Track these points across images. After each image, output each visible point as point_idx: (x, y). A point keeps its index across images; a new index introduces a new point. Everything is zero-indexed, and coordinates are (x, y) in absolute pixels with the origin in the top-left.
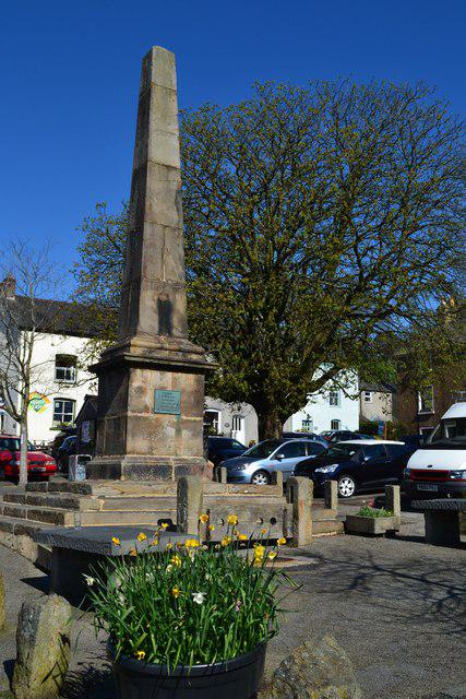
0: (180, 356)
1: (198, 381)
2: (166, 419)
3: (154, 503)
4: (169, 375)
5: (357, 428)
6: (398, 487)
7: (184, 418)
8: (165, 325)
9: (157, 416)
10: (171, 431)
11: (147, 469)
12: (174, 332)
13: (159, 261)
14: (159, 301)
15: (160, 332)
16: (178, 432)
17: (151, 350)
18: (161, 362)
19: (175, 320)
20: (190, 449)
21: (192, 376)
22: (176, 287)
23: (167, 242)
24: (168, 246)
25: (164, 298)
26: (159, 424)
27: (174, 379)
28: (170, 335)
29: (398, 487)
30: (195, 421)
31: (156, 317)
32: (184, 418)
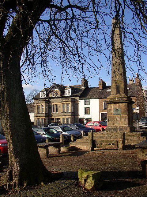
0: (120, 99)
1: (125, 105)
10: (118, 119)
16: (121, 119)
17: (112, 99)
21: (124, 104)
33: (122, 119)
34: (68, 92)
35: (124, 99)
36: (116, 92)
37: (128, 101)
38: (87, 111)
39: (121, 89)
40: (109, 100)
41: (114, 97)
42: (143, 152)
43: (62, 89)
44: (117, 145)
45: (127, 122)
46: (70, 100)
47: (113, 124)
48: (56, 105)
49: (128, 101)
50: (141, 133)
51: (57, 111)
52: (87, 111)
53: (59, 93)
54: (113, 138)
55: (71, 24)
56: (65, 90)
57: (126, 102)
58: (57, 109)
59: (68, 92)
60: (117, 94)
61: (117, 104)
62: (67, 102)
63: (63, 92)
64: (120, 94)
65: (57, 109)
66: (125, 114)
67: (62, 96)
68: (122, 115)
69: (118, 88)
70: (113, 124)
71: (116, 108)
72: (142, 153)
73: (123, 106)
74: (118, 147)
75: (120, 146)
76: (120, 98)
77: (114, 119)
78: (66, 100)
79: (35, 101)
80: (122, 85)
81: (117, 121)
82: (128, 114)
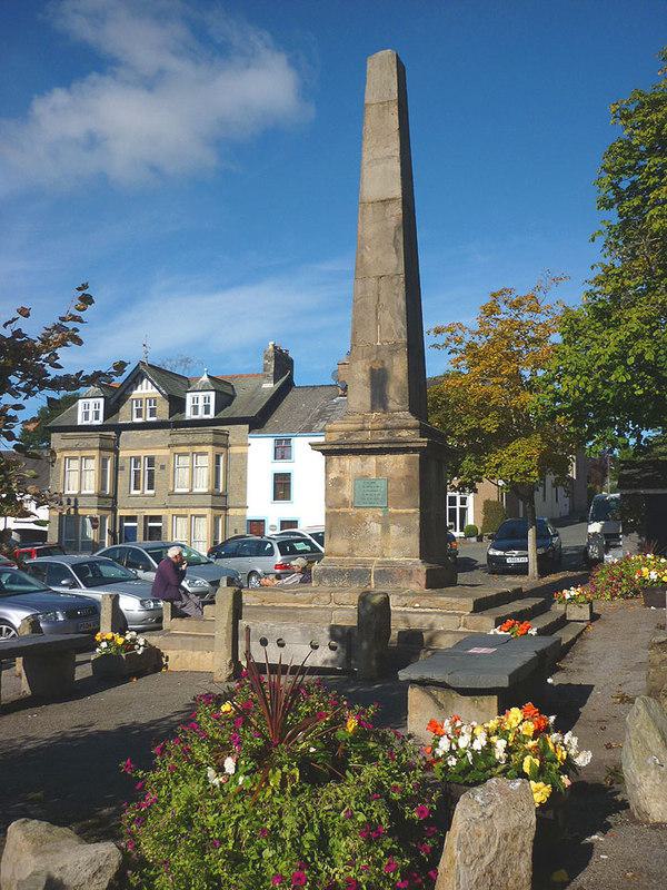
0: (385, 436)
1: (409, 463)
2: (368, 514)
3: (279, 613)
4: (373, 459)
5: (53, 435)
6: (77, 656)
7: (392, 510)
8: (379, 399)
9: (357, 511)
10: (376, 528)
11: (341, 573)
12: (391, 405)
13: (373, 323)
14: (372, 370)
15: (373, 409)
16: (386, 528)
17: (349, 433)
18: (374, 446)
19: (392, 391)
20: (401, 548)
21: (401, 458)
22: (393, 351)
23: (383, 295)
24: (383, 300)
25: (378, 366)
26: (360, 521)
27: (379, 465)
28: (385, 409)
29: (77, 656)
30: (407, 514)
31: (367, 391)
32: (392, 510)
33: (393, 528)
34: (199, 403)
35: (404, 433)
36: (368, 402)
37: (423, 442)
38: (282, 487)
40: (335, 437)
43: (175, 388)
45: (413, 541)
46: (96, 443)
48: (151, 461)
49: (423, 442)
50: (295, 530)
51: (151, 487)
52: (282, 487)
53: (163, 411)
56: (189, 397)
57: (415, 450)
58: (151, 474)
59: (199, 403)
62: (195, 444)
63: (177, 404)
65: (151, 474)
66: (404, 507)
67: (175, 421)
69: (378, 380)
73: (397, 464)
78: (191, 439)
79: (20, 457)
80: (399, 368)
82: (423, 506)
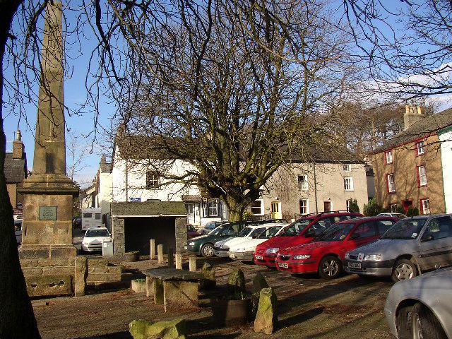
0: (55, 186)
1: (68, 200)
10: (50, 230)
16: (55, 230)
21: (64, 197)
35: (66, 185)
36: (44, 170)
39: (57, 164)
41: (42, 180)
42: (178, 288)
44: (69, 287)
47: (37, 242)
54: (67, 269)
55: (201, 58)
60: (47, 173)
61: (49, 196)
64: (53, 173)
68: (58, 221)
70: (37, 242)
71: (45, 206)
72: (175, 292)
74: (73, 291)
75: (79, 287)
76: (56, 182)
77: (40, 229)
81: (46, 234)
